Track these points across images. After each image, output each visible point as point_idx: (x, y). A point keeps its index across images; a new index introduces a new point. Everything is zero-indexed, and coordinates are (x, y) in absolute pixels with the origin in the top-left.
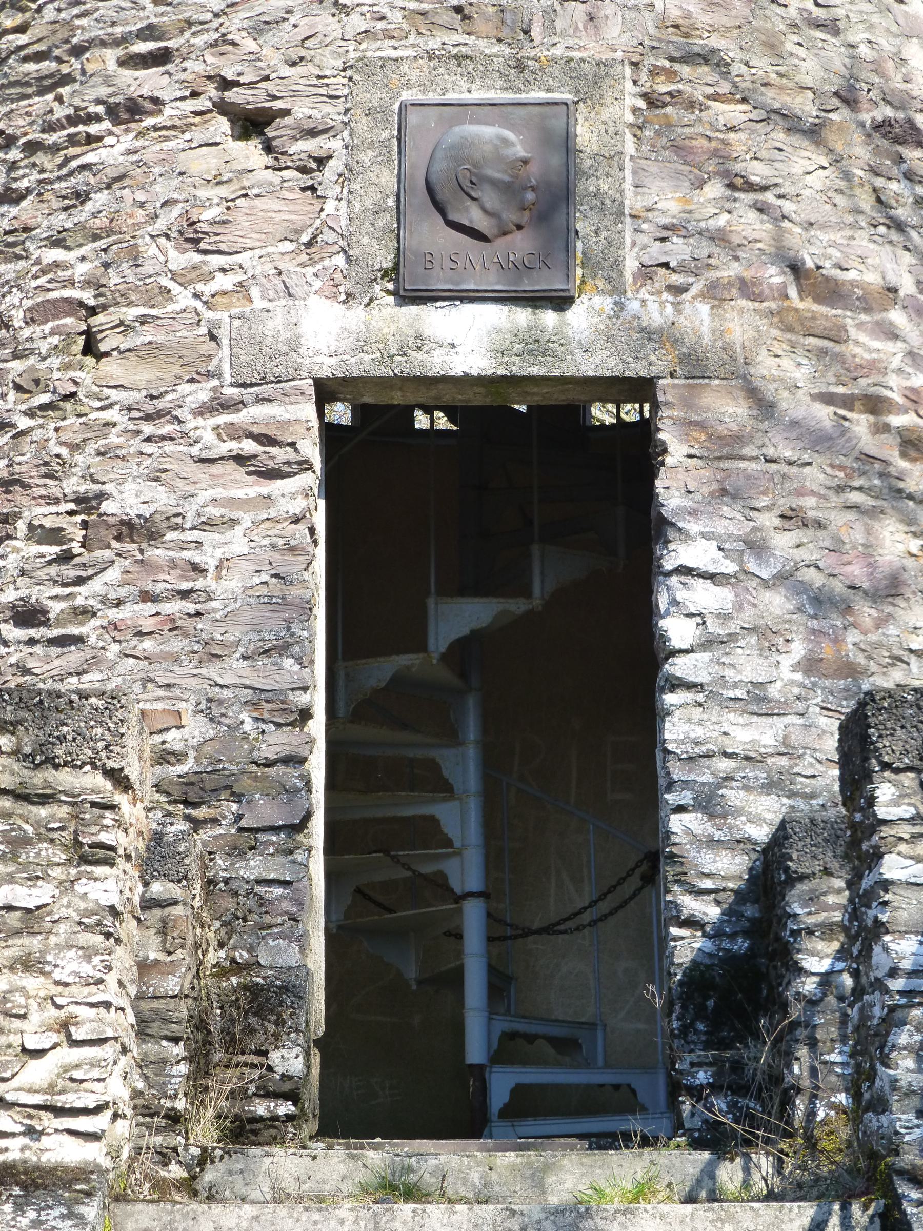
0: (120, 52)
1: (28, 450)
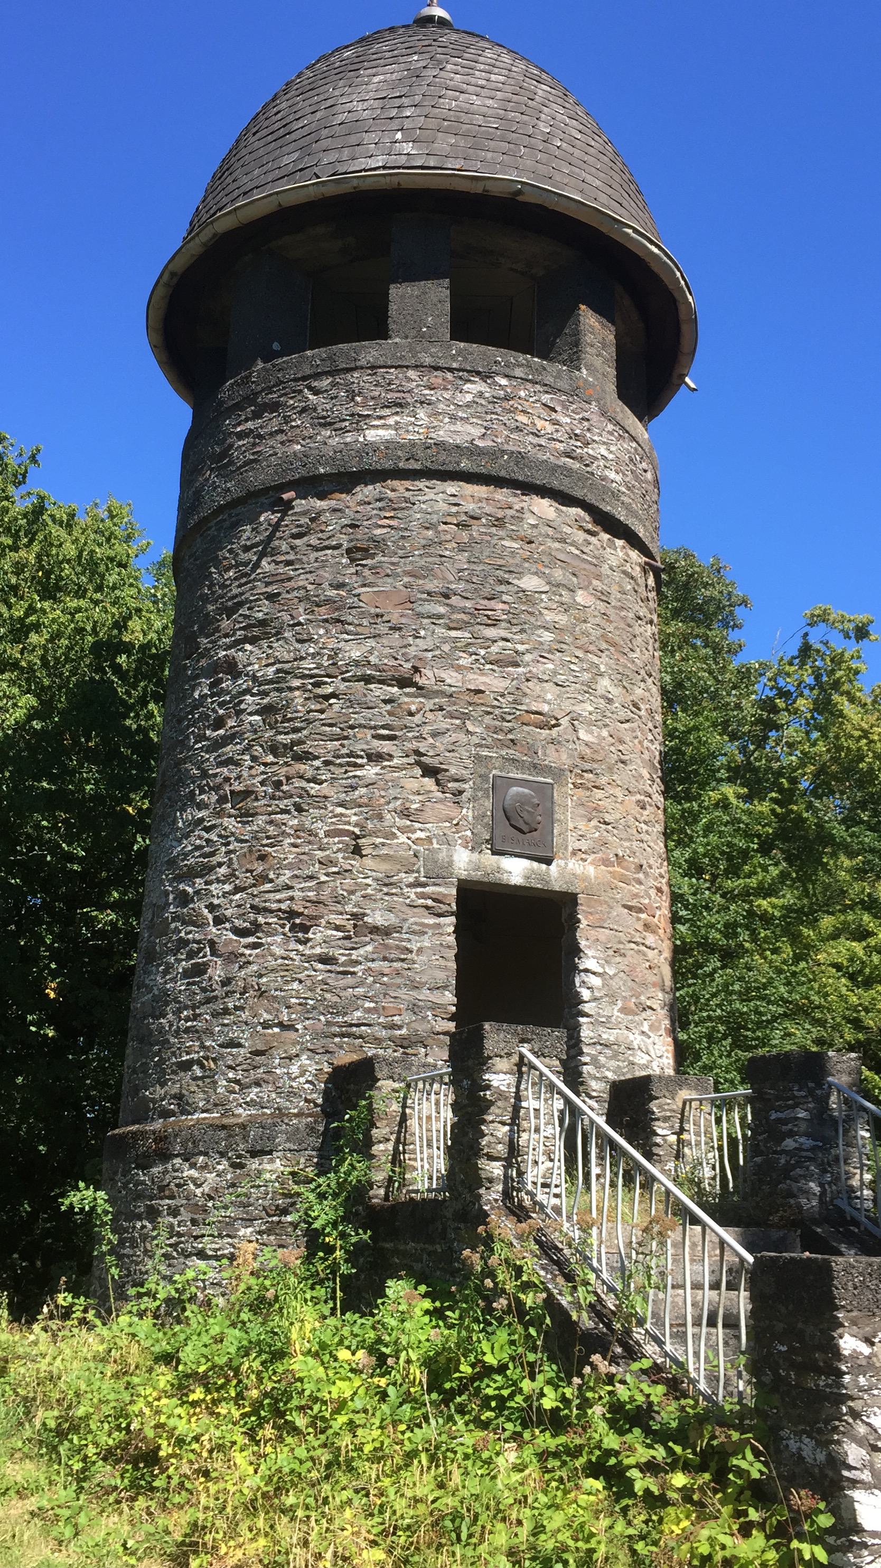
0: (372, 732)
1: (327, 891)
